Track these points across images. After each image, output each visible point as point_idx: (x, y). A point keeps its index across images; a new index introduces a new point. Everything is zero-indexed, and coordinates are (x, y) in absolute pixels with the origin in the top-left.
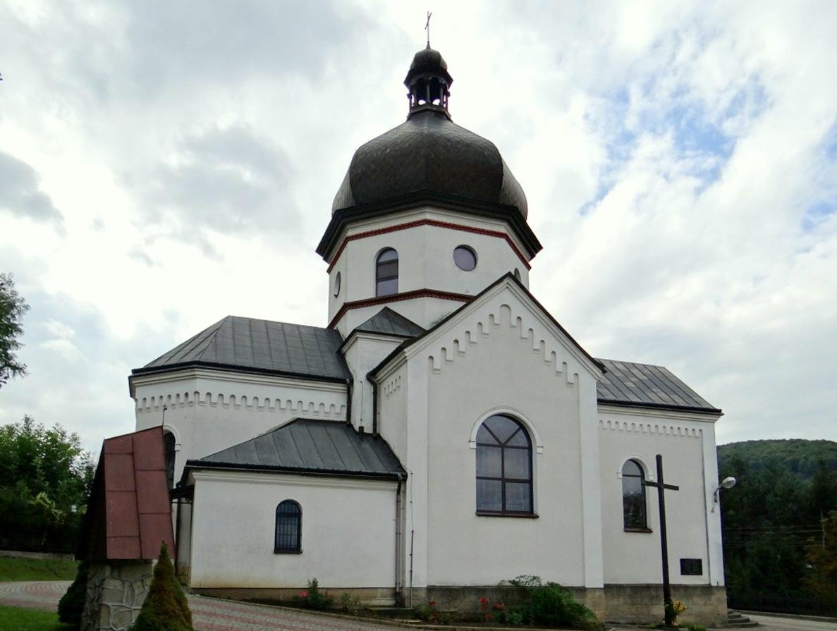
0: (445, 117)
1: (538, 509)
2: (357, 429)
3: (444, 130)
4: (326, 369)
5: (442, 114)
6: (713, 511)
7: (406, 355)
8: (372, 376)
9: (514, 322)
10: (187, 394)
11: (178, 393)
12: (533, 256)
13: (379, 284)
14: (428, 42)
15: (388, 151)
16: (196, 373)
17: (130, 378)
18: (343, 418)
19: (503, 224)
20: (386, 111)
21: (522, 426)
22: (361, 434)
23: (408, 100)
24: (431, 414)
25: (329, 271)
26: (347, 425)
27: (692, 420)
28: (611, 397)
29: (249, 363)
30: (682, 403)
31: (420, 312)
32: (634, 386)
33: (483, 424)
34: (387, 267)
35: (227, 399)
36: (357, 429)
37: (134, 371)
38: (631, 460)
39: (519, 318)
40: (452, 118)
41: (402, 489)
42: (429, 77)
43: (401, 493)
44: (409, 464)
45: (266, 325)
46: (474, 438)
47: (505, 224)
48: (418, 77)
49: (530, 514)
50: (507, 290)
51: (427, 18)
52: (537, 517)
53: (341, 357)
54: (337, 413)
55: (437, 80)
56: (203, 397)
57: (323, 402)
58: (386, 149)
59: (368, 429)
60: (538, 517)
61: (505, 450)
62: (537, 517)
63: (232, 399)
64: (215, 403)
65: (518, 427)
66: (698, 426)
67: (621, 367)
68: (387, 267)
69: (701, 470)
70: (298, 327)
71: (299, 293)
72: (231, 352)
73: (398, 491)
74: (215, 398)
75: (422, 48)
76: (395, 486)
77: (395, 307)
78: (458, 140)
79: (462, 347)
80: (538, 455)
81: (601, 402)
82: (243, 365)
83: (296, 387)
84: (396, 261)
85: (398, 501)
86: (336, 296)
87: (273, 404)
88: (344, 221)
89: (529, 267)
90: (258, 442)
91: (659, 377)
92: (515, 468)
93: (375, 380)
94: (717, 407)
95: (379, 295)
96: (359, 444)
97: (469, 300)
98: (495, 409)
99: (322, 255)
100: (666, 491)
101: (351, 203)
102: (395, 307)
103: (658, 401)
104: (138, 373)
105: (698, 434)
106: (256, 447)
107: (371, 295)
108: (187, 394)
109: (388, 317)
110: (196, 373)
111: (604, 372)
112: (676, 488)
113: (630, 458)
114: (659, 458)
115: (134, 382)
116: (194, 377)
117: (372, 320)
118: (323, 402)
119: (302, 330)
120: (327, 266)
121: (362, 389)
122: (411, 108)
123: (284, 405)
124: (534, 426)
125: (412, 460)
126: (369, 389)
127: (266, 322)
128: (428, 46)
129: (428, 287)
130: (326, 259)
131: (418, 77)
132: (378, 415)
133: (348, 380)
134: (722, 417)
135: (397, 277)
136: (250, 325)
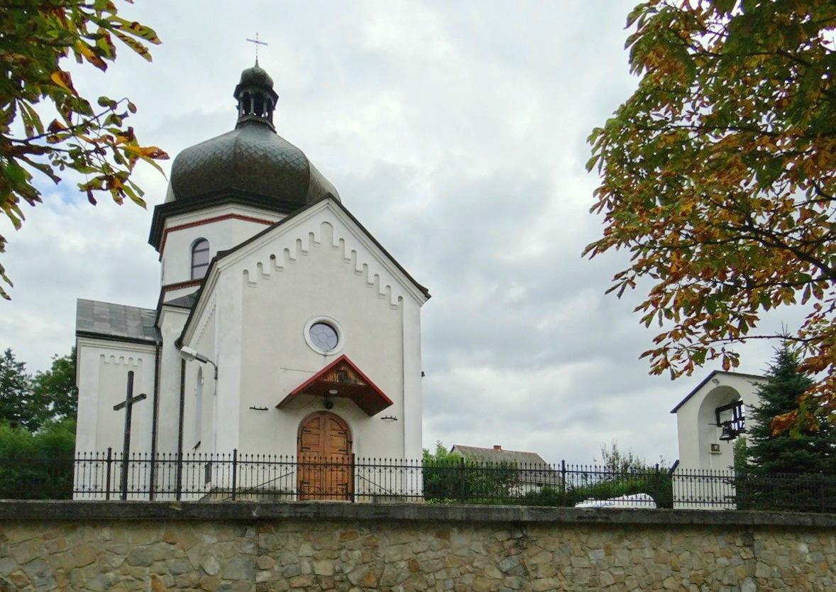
0: (268, 127)
5: (267, 125)
14: (257, 61)
20: (214, 118)
23: (237, 111)
40: (276, 130)
42: (256, 94)
53: (157, 329)
75: (251, 65)
88: (163, 215)
99: (154, 246)
101: (172, 199)
107: (187, 278)
130: (157, 250)
133: (158, 342)
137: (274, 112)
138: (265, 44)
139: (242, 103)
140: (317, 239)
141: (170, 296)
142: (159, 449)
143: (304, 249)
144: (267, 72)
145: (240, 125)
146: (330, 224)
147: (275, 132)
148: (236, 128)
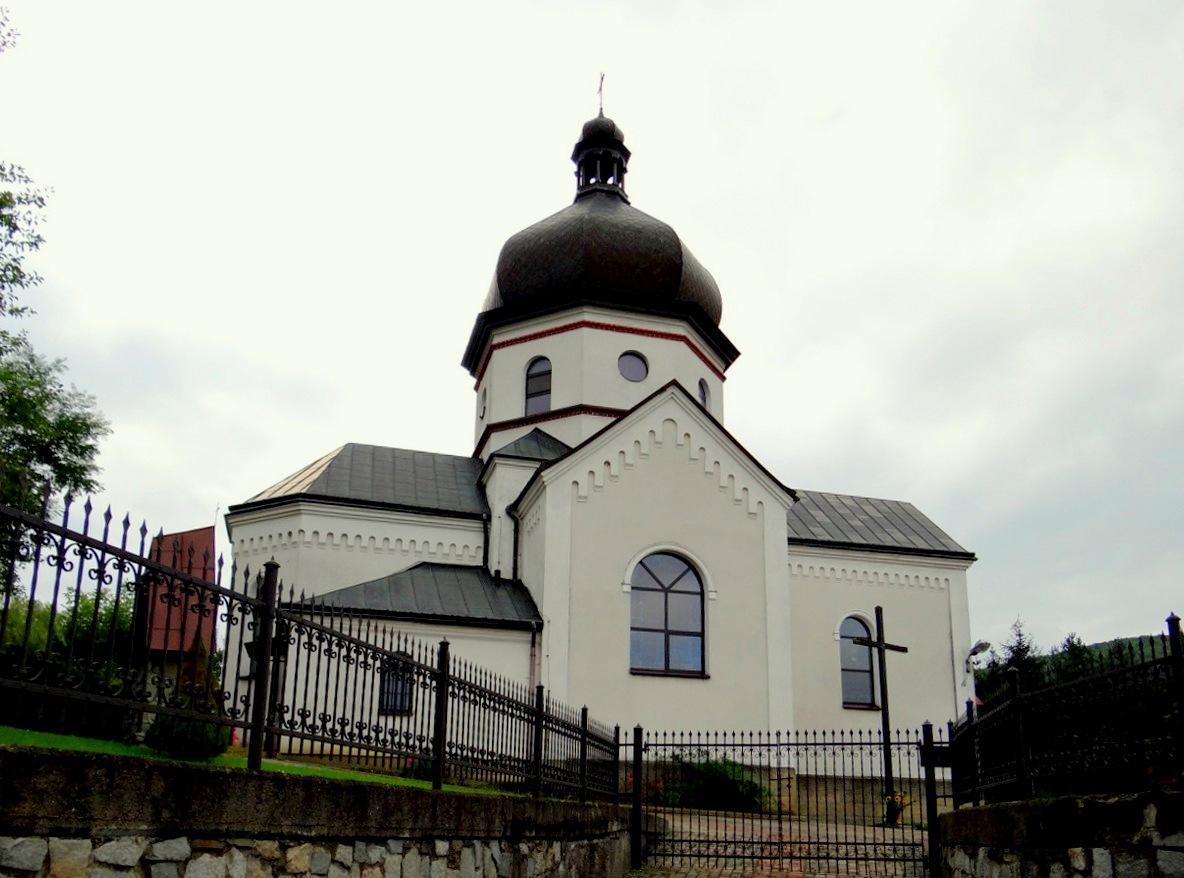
0: (619, 198)
1: (710, 670)
2: (493, 573)
3: (618, 216)
4: (460, 504)
5: (618, 196)
6: (964, 684)
7: (544, 479)
8: (513, 511)
9: (681, 439)
10: (290, 534)
11: (280, 532)
12: (728, 365)
13: (530, 400)
15: (542, 240)
16: (302, 508)
17: (226, 516)
18: (479, 562)
19: (681, 324)
20: (550, 193)
21: (692, 567)
22: (497, 580)
23: (576, 179)
24: (579, 547)
25: (477, 388)
26: (482, 571)
27: (935, 566)
28: (827, 538)
29: (346, 493)
30: (922, 545)
31: (565, 431)
32: (829, 521)
33: (641, 562)
34: (538, 378)
35: (337, 539)
36: (493, 573)
37: (231, 508)
38: (848, 618)
39: (687, 435)
40: (629, 200)
41: (537, 640)
42: (601, 153)
43: (537, 646)
44: (546, 611)
45: (433, 459)
46: (628, 580)
47: (684, 324)
48: (585, 152)
49: (702, 675)
50: (672, 402)
51: (600, 79)
52: (708, 677)
53: (481, 489)
54: (470, 556)
55: (610, 154)
56: (308, 536)
57: (456, 543)
58: (540, 239)
59: (507, 574)
60: (709, 677)
61: (669, 595)
62: (708, 677)
63: (330, 537)
64: (323, 544)
65: (686, 567)
66: (942, 574)
67: (849, 502)
68: (538, 378)
69: (948, 632)
70: (433, 455)
71: (443, 418)
72: (359, 484)
73: (533, 644)
74: (323, 538)
75: (593, 116)
76: (528, 636)
77: (547, 427)
78: (626, 224)
79: (615, 469)
80: (710, 602)
81: (792, 541)
82: (358, 498)
83: (434, 526)
84: (549, 372)
85: (533, 655)
86: (482, 418)
87: (392, 544)
89: (723, 379)
90: (368, 588)
91: (902, 514)
92: (682, 612)
93: (517, 515)
94: (970, 551)
95: (529, 414)
96: (494, 594)
97: (620, 415)
98: (655, 545)
100: (888, 653)
102: (547, 427)
103: (889, 542)
104: (236, 511)
105: (943, 584)
106: (365, 591)
107: (518, 412)
108: (290, 534)
109: (537, 440)
110: (302, 508)
111: (796, 499)
112: (904, 650)
113: (848, 615)
114: (879, 611)
115: (230, 521)
116: (298, 513)
117: (516, 443)
118: (456, 543)
119: (438, 460)
120: (474, 381)
121: (501, 526)
122: (579, 188)
123: (406, 545)
124: (706, 567)
125: (550, 606)
126: (509, 525)
127: (394, 450)
128: (601, 114)
129: (585, 402)
130: (473, 373)
131: (585, 152)
132: (519, 557)
134: (975, 562)
135: (548, 391)
136: (373, 454)
137: (626, 177)
138: (601, 89)
139: (259, 620)
140: (658, 437)
141: (498, 442)
142: (893, 729)
143: (643, 451)
144: (616, 123)
145: (580, 198)
146: (672, 420)
147: (629, 204)
148: (576, 201)
